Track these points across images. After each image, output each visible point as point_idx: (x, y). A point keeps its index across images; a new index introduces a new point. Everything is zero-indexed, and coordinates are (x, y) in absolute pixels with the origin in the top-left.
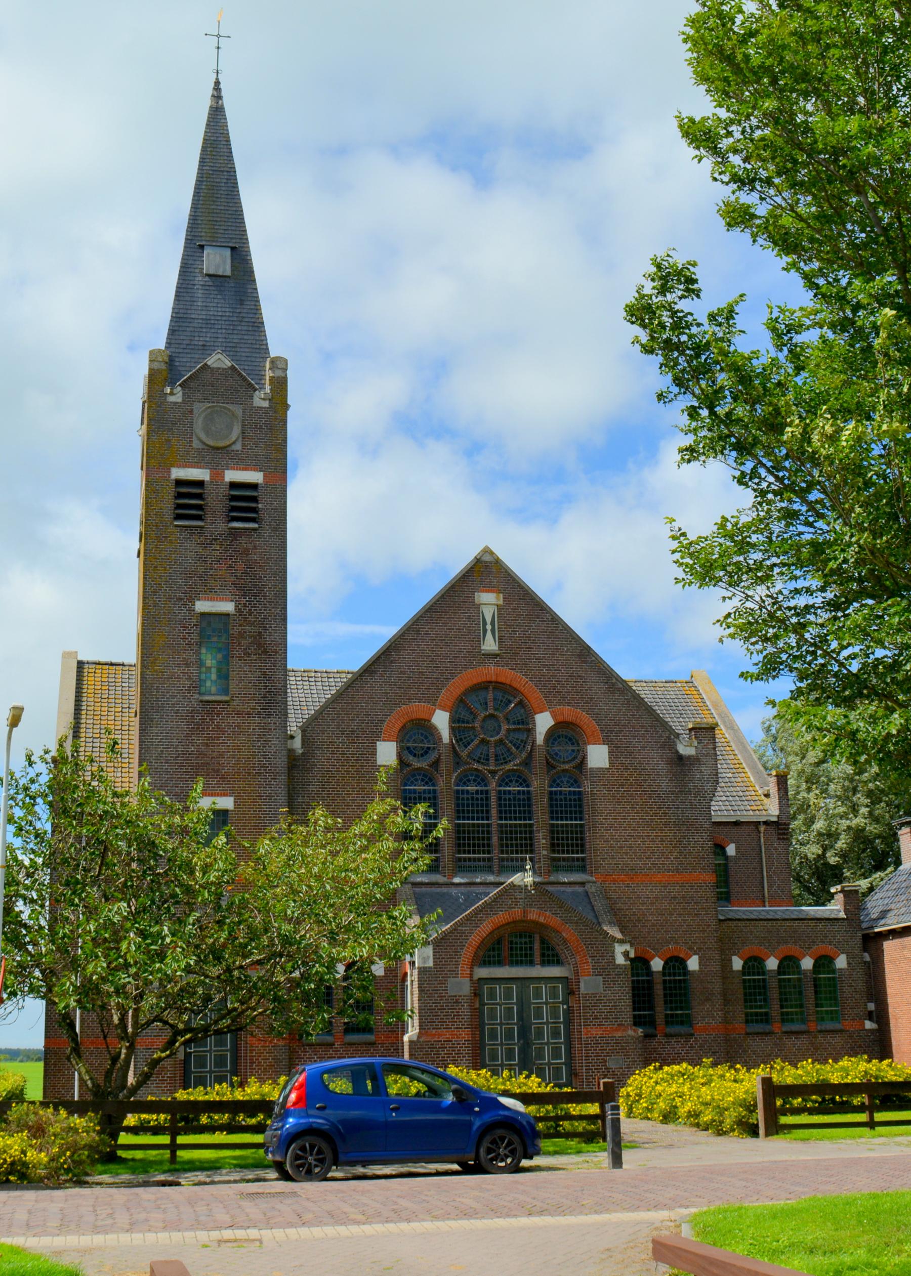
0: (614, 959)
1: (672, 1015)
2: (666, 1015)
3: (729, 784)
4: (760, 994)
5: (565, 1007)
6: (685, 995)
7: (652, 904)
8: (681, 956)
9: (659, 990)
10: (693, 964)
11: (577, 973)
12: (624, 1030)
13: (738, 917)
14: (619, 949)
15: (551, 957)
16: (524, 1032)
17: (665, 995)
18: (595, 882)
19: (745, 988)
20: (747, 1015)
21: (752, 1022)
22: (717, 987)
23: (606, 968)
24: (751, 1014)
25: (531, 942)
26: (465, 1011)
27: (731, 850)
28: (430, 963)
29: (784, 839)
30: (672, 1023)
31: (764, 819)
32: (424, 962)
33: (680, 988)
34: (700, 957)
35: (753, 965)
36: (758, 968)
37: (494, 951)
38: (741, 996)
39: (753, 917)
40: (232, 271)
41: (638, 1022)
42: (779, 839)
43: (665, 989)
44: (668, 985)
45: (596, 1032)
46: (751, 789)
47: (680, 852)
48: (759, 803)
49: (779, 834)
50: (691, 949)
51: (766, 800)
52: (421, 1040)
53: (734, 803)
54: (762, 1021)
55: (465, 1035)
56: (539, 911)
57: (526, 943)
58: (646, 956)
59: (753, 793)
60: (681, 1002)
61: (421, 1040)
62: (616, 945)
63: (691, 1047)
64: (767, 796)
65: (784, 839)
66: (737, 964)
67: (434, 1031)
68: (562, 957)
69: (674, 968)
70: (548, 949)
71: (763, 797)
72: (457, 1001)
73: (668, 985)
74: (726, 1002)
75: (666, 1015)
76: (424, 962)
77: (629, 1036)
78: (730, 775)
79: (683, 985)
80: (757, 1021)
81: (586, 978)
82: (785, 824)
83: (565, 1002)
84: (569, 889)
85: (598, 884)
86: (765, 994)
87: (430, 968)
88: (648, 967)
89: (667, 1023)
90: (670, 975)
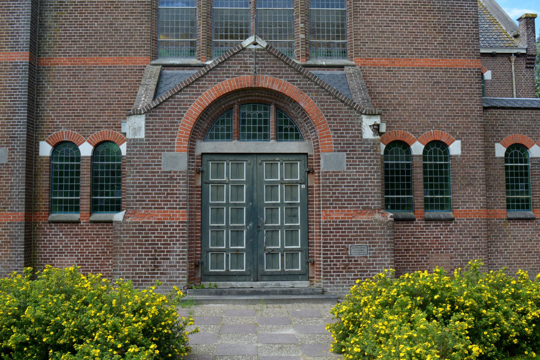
0: (361, 133)
1: (432, 200)
2: (426, 200)
3: (487, 31)
4: (522, 181)
5: (303, 186)
6: (446, 179)
7: (414, 88)
8: (443, 140)
9: (418, 174)
10: (455, 148)
11: (317, 149)
12: (370, 214)
13: (502, 105)
14: (367, 122)
15: (288, 130)
16: (254, 214)
17: (425, 180)
18: (354, 66)
19: (507, 175)
20: (508, 200)
21: (513, 207)
22: (480, 172)
23: (351, 144)
24: (513, 200)
25: (266, 115)
26: (181, 188)
27: (488, 75)
28: (142, 135)
29: (530, 68)
30: (432, 207)
31: (515, 51)
32: (135, 134)
33: (441, 173)
34: (462, 142)
35: (516, 153)
36: (521, 156)
37: (216, 119)
38: (503, 183)
39: (516, 105)
40: (386, 130)
41: (389, 204)
42: (527, 67)
43: (425, 173)
44: (428, 169)
45: (337, 215)
46: (503, 34)
47: (444, 38)
48: (510, 42)
49: (527, 64)
50: (453, 133)
51: (516, 41)
52: (128, 220)
53: (490, 42)
54: (523, 207)
55: (180, 216)
56: (272, 77)
57: (260, 115)
58: (406, 140)
59: (506, 36)
60: (441, 186)
61: (128, 220)
62: (364, 117)
63: (451, 231)
64: (516, 36)
65: (530, 68)
66: (500, 151)
67: (143, 211)
68: (302, 132)
69: (435, 153)
70: (286, 122)
71: (513, 39)
72: (171, 178)
73: (428, 169)
74: (488, 187)
75: (426, 200)
76: (135, 134)
77: (376, 221)
78: (487, 26)
79: (444, 169)
80: (518, 207)
81: (327, 154)
82: (532, 55)
83: (304, 181)
84: (327, 72)
85: (358, 67)
86: (527, 181)
87: (141, 140)
88: (409, 151)
89: (426, 207)
90: (430, 160)
